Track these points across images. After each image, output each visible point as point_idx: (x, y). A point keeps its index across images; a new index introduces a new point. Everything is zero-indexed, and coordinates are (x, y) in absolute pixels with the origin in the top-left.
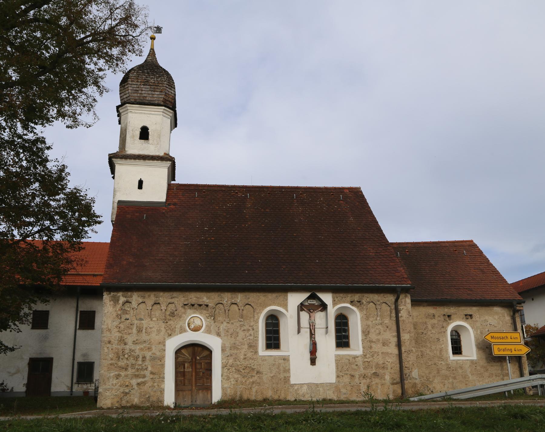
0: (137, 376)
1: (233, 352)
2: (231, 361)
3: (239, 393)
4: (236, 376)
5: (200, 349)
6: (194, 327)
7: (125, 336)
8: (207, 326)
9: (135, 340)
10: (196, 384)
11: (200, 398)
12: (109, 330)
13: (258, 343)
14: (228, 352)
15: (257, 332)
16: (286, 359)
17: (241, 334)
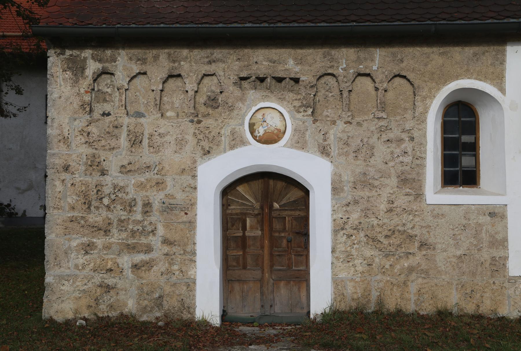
0: (132, 248)
1: (362, 194)
2: (355, 216)
3: (374, 295)
4: (368, 252)
5: (280, 184)
6: (266, 132)
7: (103, 155)
9: (125, 163)
10: (272, 266)
11: (281, 300)
12: (65, 140)
13: (424, 174)
14: (348, 195)
15: (423, 144)
16: (497, 214)
17: (382, 151)
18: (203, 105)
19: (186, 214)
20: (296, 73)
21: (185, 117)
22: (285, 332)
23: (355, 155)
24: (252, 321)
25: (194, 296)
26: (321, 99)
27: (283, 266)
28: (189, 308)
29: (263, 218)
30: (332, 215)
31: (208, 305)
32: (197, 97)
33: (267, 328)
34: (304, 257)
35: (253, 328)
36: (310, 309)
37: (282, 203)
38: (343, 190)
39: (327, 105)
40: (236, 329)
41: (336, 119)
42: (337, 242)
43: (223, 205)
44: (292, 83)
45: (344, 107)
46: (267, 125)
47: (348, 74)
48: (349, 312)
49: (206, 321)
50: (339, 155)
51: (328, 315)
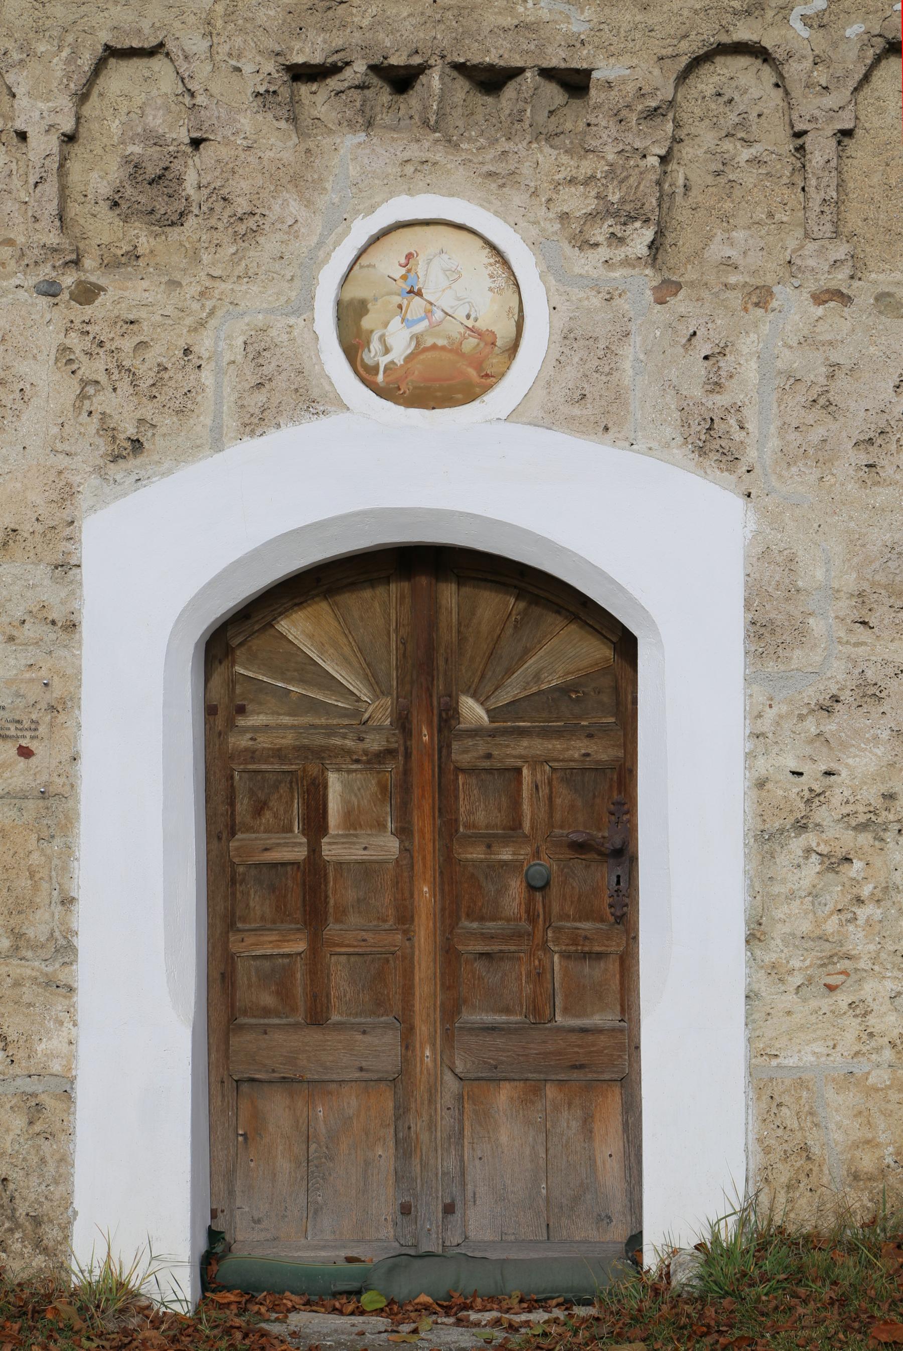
5: (492, 606)
6: (419, 349)
8: (568, 337)
10: (451, 1011)
11: (500, 1175)
14: (827, 657)
18: (104, 206)
19: (25, 752)
20: (575, 43)
21: (12, 265)
22: (516, 1339)
23: (863, 458)
24: (355, 1285)
25: (65, 1160)
26: (699, 177)
27: (507, 1010)
28: (37, 1221)
29: (407, 772)
30: (750, 756)
31: (132, 1209)
32: (75, 167)
33: (426, 1322)
34: (613, 966)
35: (358, 1320)
36: (640, 1222)
37: (504, 697)
38: (801, 632)
39: (728, 205)
40: (275, 1329)
41: (770, 279)
42: (776, 889)
43: (210, 710)
44: (553, 93)
45: (812, 215)
46: (429, 313)
47: (835, 45)
48: (836, 1242)
49: (121, 1285)
50: (787, 458)
51: (728, 1253)
